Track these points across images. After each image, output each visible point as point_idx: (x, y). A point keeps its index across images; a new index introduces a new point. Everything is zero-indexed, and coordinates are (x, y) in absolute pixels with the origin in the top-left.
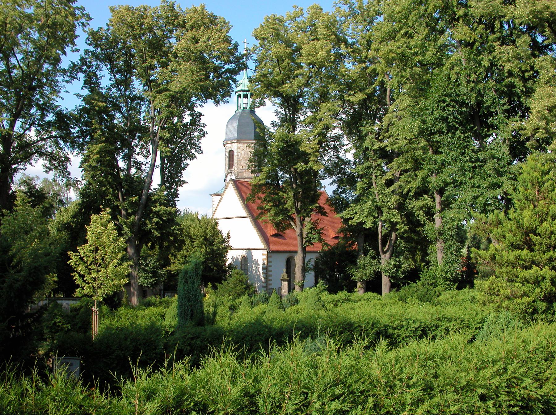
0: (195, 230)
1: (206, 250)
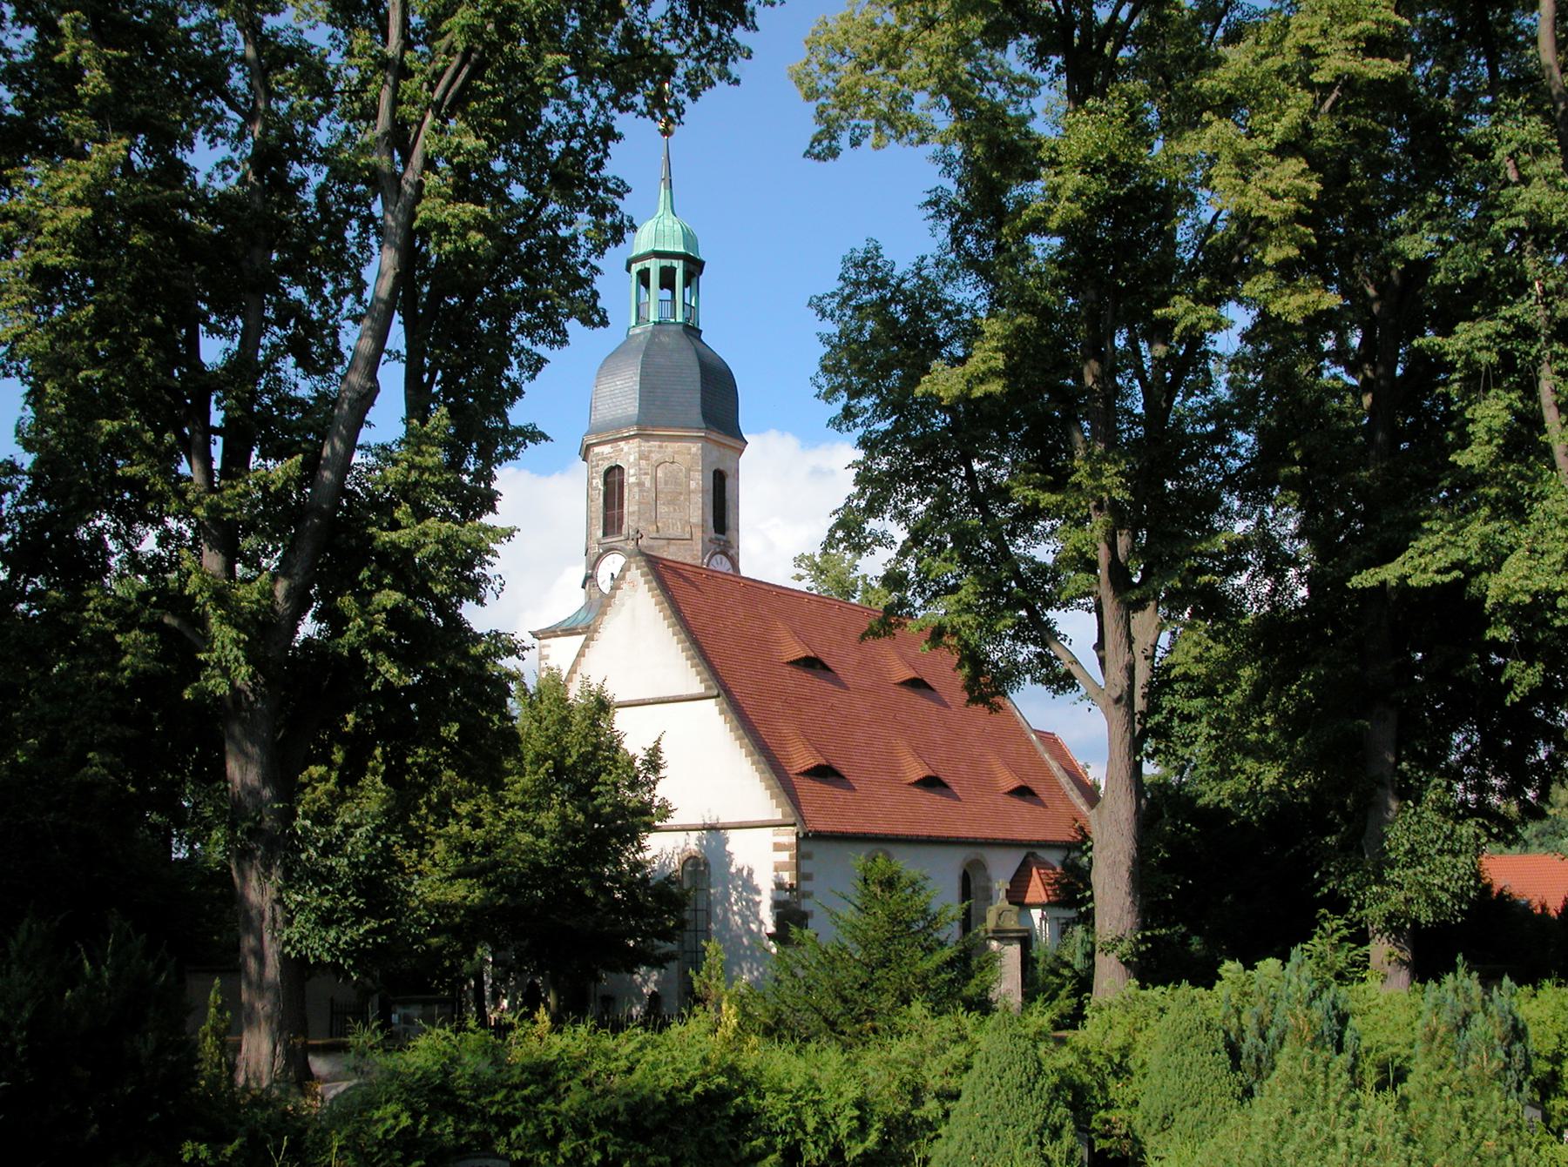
1: (563, 818)
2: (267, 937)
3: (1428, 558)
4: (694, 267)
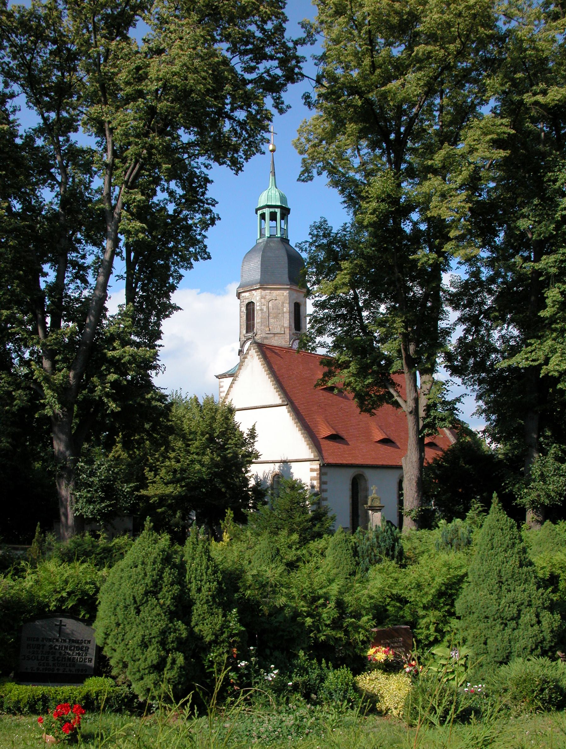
0: (192, 422)
1: (212, 459)
2: (69, 508)
3: (528, 355)
4: (285, 212)
